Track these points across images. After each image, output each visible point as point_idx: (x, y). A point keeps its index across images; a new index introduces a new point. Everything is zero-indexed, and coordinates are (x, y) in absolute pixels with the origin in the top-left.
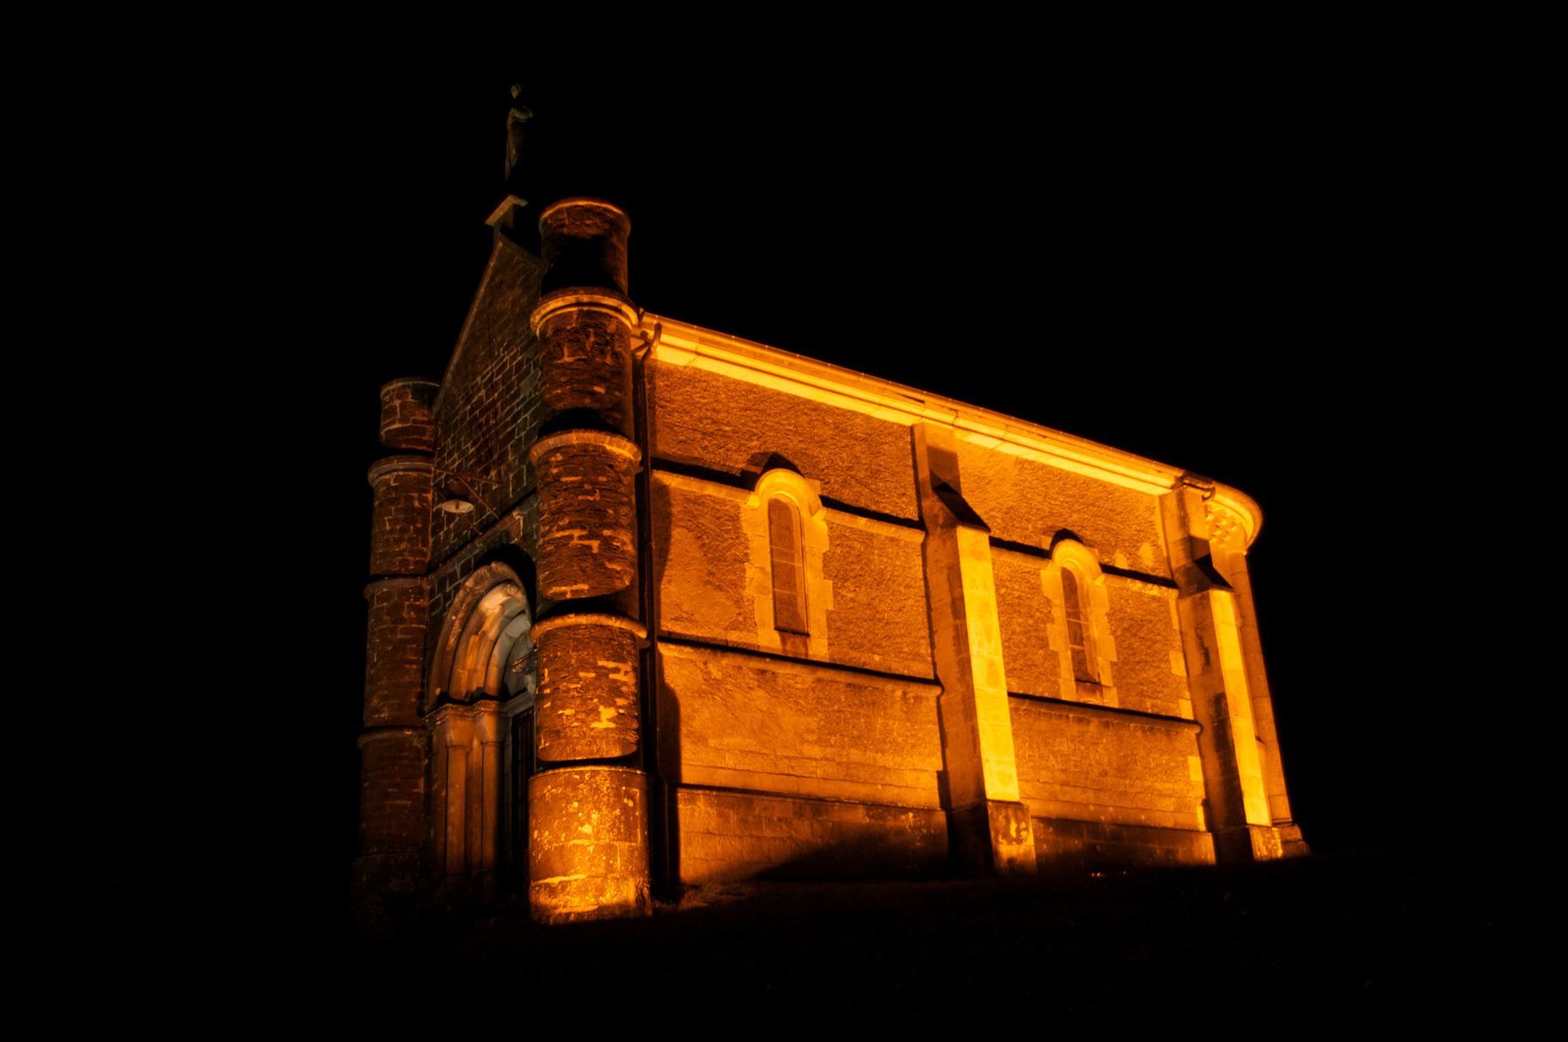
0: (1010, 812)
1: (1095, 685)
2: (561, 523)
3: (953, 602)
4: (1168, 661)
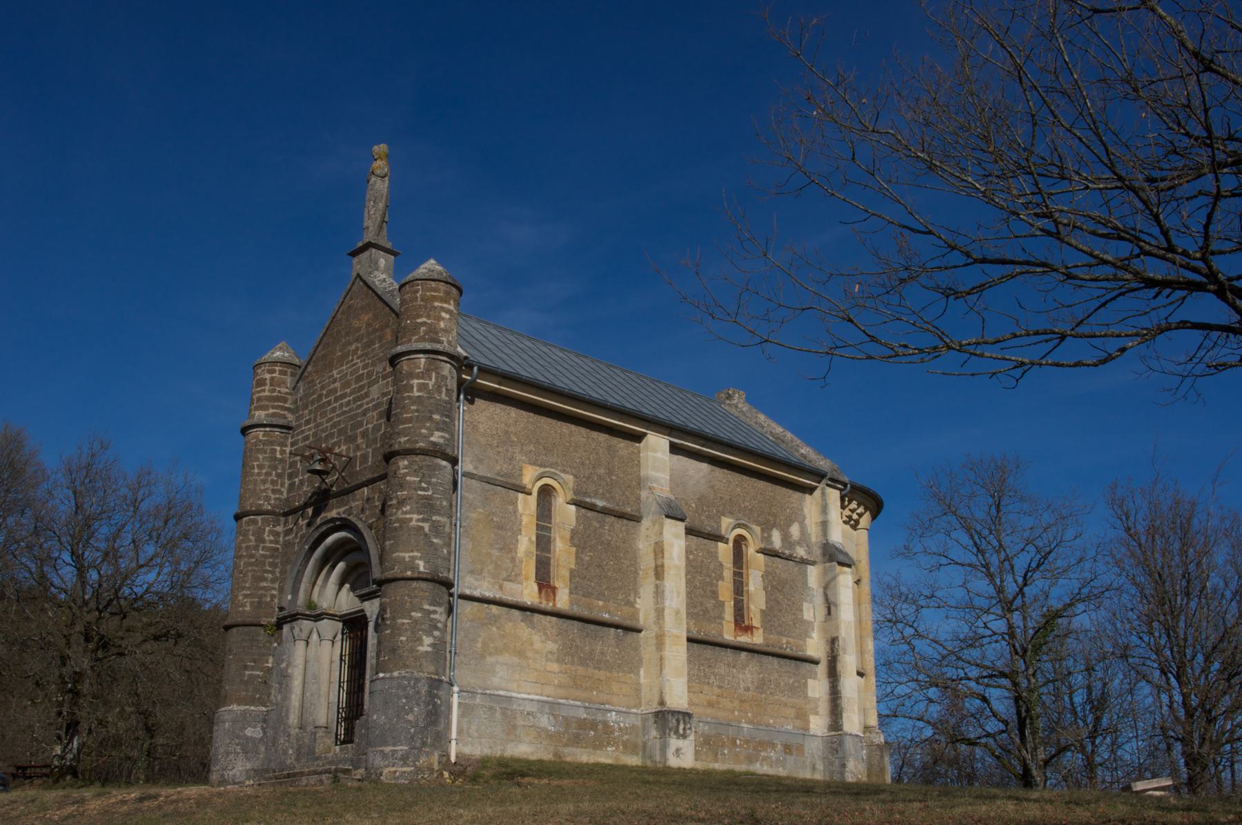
0: (681, 717)
1: (749, 629)
2: (405, 509)
3: (656, 567)
4: (802, 610)
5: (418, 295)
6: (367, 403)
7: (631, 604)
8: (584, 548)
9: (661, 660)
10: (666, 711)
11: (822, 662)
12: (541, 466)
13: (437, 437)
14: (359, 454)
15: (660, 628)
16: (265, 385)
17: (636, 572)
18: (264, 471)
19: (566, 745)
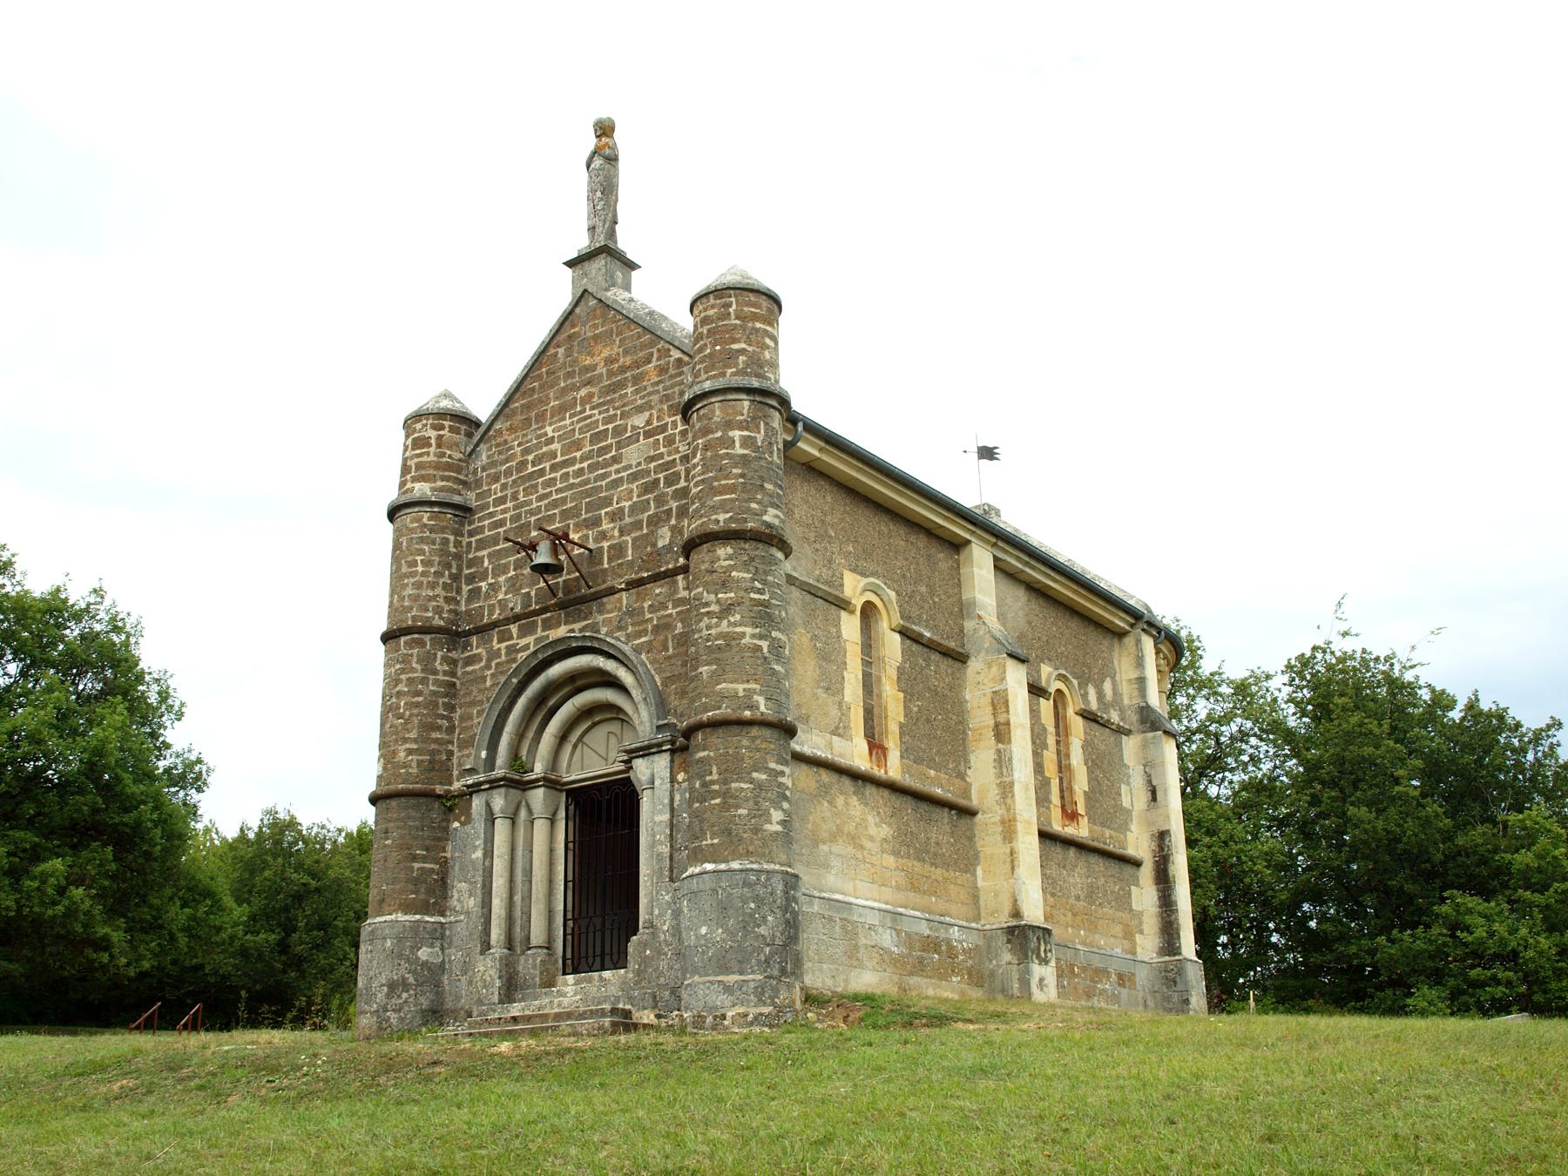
1: (1071, 816)
3: (997, 725)
5: (731, 310)
6: (618, 471)
7: (962, 776)
8: (912, 695)
9: (1012, 854)
10: (1026, 925)
11: (1144, 865)
12: (863, 574)
13: (771, 516)
14: (605, 544)
15: (1008, 810)
16: (430, 445)
17: (964, 732)
18: (432, 570)
19: (911, 974)
